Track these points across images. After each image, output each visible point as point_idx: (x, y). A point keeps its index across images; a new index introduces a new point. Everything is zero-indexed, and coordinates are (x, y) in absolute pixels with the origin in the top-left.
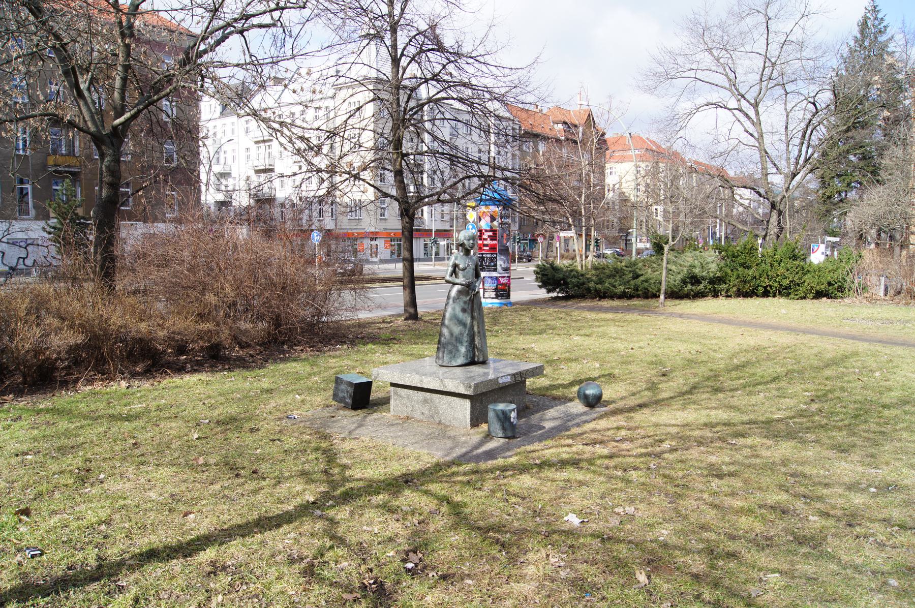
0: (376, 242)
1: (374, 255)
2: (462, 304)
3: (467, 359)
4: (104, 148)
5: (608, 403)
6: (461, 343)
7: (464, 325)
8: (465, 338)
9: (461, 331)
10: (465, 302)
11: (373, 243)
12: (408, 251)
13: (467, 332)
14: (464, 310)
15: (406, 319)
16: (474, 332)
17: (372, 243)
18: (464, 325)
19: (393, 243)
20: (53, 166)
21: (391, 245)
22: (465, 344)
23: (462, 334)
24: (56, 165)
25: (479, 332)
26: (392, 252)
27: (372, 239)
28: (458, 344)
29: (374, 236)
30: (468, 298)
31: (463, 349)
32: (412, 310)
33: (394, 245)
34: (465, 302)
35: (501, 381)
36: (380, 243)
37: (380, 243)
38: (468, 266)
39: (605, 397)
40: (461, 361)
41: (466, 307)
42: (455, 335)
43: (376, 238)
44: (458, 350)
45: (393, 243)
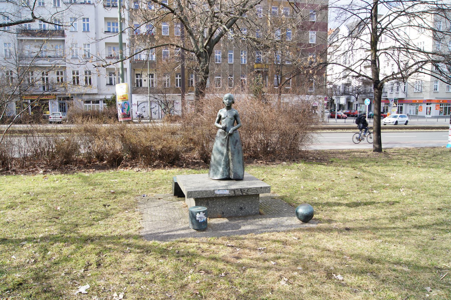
0: (430, 106)
1: (428, 114)
2: (221, 140)
3: (223, 176)
4: (200, 58)
5: (319, 221)
6: (220, 165)
7: (222, 154)
8: (223, 163)
9: (220, 158)
10: (223, 140)
11: (429, 106)
12: (376, 109)
13: (223, 159)
14: (223, 145)
15: (374, 151)
16: (229, 160)
17: (427, 106)
18: (222, 154)
19: (441, 107)
20: (256, 69)
21: (440, 108)
22: (222, 166)
23: (220, 160)
24: (257, 68)
25: (232, 160)
26: (440, 112)
27: (427, 104)
28: (218, 166)
29: (429, 102)
30: (225, 137)
31: (221, 169)
32: (377, 146)
33: (442, 108)
34: (223, 140)
35: (217, 192)
36: (433, 106)
37: (433, 106)
38: (227, 116)
39: (315, 216)
40: (219, 177)
41: (223, 143)
42: (216, 160)
43: (430, 104)
44: (218, 170)
45: (441, 107)
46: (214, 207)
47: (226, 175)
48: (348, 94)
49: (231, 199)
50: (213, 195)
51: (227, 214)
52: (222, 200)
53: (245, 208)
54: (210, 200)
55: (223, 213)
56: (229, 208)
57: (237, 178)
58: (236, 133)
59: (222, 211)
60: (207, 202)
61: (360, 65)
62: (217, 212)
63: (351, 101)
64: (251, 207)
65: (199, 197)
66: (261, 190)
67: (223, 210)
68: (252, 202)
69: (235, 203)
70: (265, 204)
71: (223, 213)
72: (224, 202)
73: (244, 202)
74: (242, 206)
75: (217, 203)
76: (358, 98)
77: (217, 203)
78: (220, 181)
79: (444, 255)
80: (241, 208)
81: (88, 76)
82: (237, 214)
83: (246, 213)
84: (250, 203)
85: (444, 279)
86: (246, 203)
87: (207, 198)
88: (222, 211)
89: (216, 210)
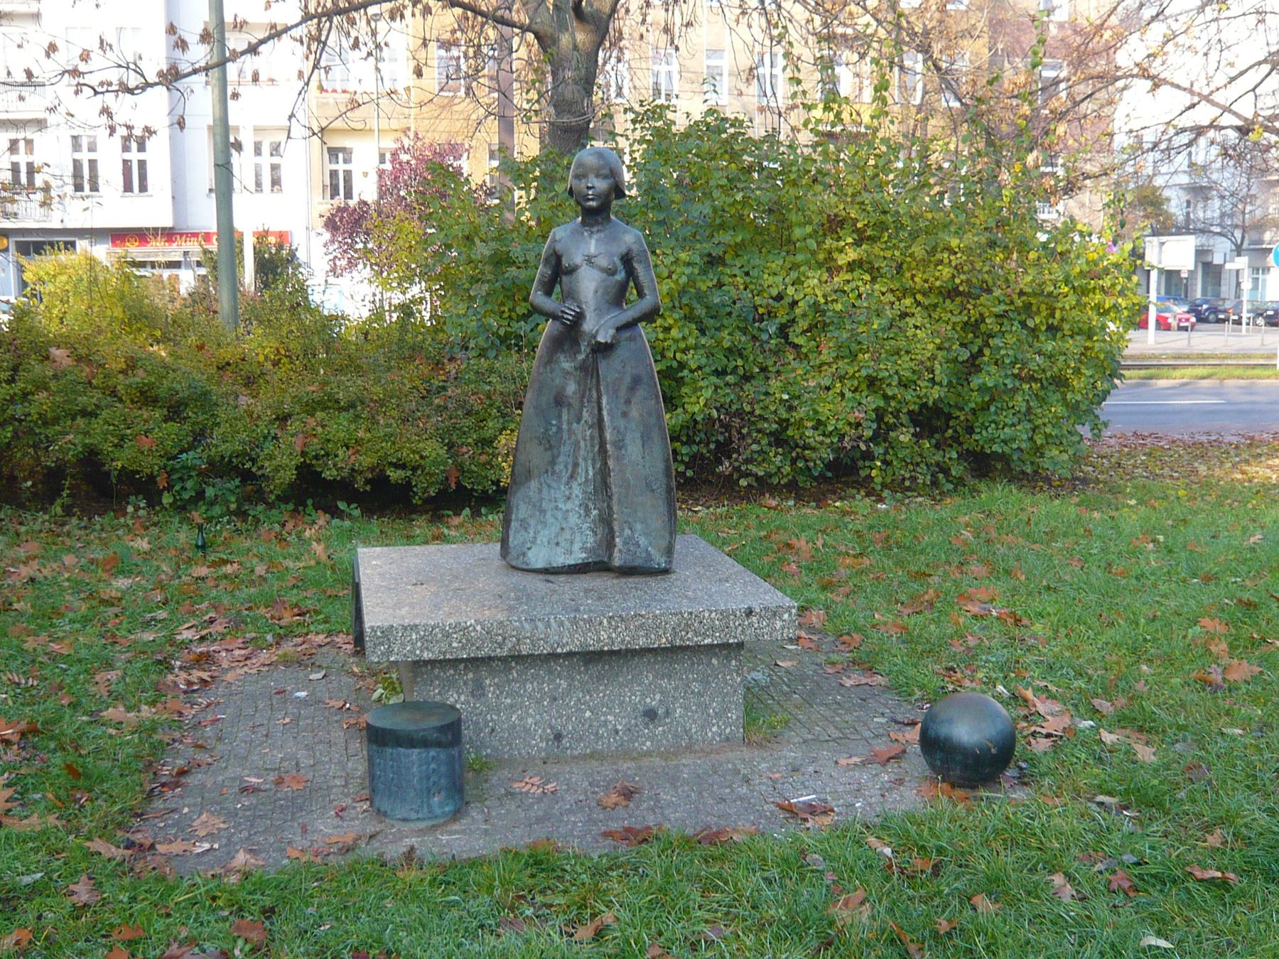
46: (512, 706)
47: (583, 549)
48: (1202, 231)
49: (595, 669)
50: (501, 646)
51: (581, 739)
52: (550, 672)
53: (667, 714)
54: (493, 674)
55: (558, 737)
56: (588, 714)
57: (638, 562)
58: (631, 339)
59: (551, 727)
60: (475, 681)
61: (1254, 90)
62: (527, 731)
63: (1218, 260)
64: (699, 705)
65: (427, 655)
66: (751, 625)
67: (558, 724)
68: (705, 682)
69: (621, 685)
70: (785, 694)
71: (558, 737)
72: (564, 684)
73: (664, 682)
74: (653, 701)
75: (529, 686)
76: (1245, 245)
77: (529, 686)
78: (551, 578)
79: (1122, 684)
80: (651, 715)
81: (84, 156)
82: (631, 741)
83: (676, 736)
84: (696, 687)
85: (643, 329)
86: (676, 689)
87: (474, 663)
88: (551, 727)
89: (521, 718)
